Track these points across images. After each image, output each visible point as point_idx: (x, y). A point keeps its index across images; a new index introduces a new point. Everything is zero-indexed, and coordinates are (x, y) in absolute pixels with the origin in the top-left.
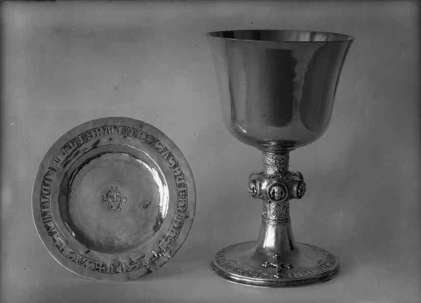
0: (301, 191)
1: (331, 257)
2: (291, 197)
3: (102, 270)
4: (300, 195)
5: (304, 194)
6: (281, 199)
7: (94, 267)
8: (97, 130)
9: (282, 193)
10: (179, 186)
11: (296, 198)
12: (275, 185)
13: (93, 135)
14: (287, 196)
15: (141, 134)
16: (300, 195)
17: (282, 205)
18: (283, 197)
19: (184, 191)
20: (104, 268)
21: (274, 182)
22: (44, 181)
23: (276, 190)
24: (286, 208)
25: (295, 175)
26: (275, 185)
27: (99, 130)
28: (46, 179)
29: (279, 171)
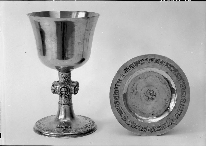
0: (76, 91)
1: (93, 122)
2: (72, 94)
3: (144, 130)
4: (75, 92)
5: (77, 92)
6: (66, 94)
7: (140, 128)
8: (142, 60)
9: (66, 92)
10: (183, 89)
11: (73, 94)
12: (63, 87)
13: (141, 63)
14: (68, 93)
15: (165, 63)
16: (75, 92)
17: (67, 97)
18: (67, 93)
19: (185, 92)
20: (145, 129)
21: (63, 86)
22: (115, 86)
23: (63, 90)
24: (70, 99)
25: (74, 82)
26: (63, 87)
27: (143, 60)
28: (117, 85)
29: (66, 81)
